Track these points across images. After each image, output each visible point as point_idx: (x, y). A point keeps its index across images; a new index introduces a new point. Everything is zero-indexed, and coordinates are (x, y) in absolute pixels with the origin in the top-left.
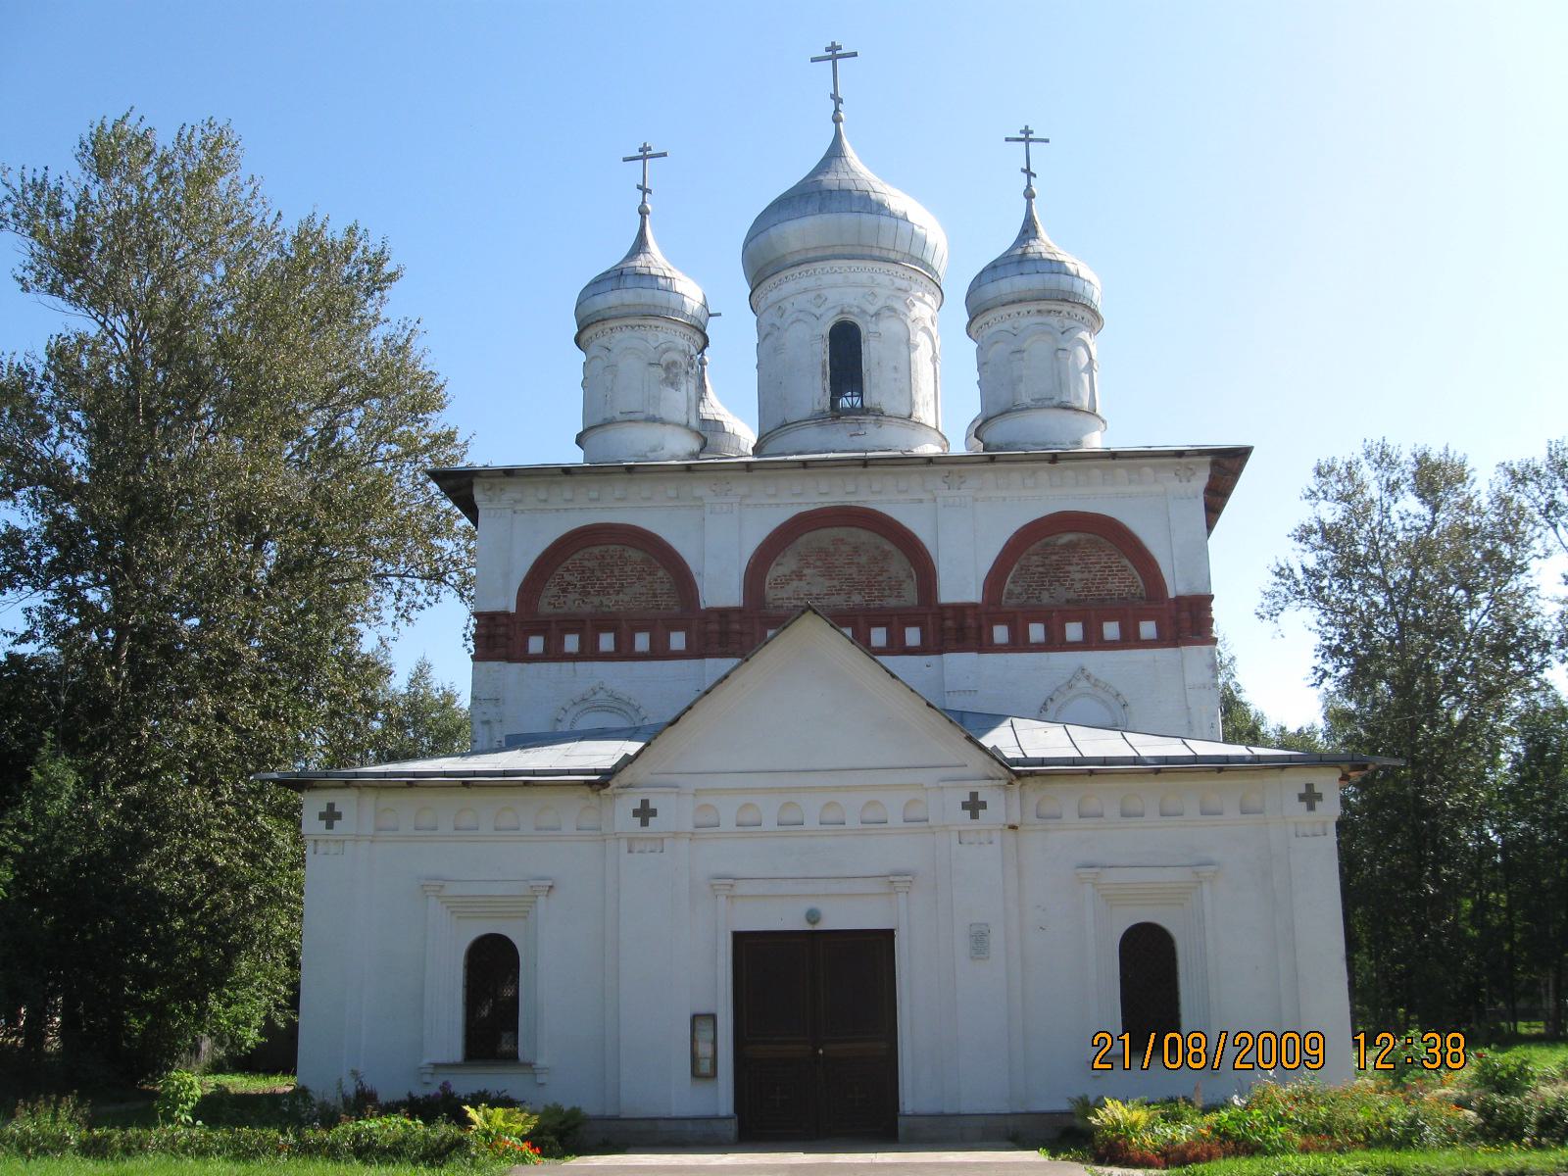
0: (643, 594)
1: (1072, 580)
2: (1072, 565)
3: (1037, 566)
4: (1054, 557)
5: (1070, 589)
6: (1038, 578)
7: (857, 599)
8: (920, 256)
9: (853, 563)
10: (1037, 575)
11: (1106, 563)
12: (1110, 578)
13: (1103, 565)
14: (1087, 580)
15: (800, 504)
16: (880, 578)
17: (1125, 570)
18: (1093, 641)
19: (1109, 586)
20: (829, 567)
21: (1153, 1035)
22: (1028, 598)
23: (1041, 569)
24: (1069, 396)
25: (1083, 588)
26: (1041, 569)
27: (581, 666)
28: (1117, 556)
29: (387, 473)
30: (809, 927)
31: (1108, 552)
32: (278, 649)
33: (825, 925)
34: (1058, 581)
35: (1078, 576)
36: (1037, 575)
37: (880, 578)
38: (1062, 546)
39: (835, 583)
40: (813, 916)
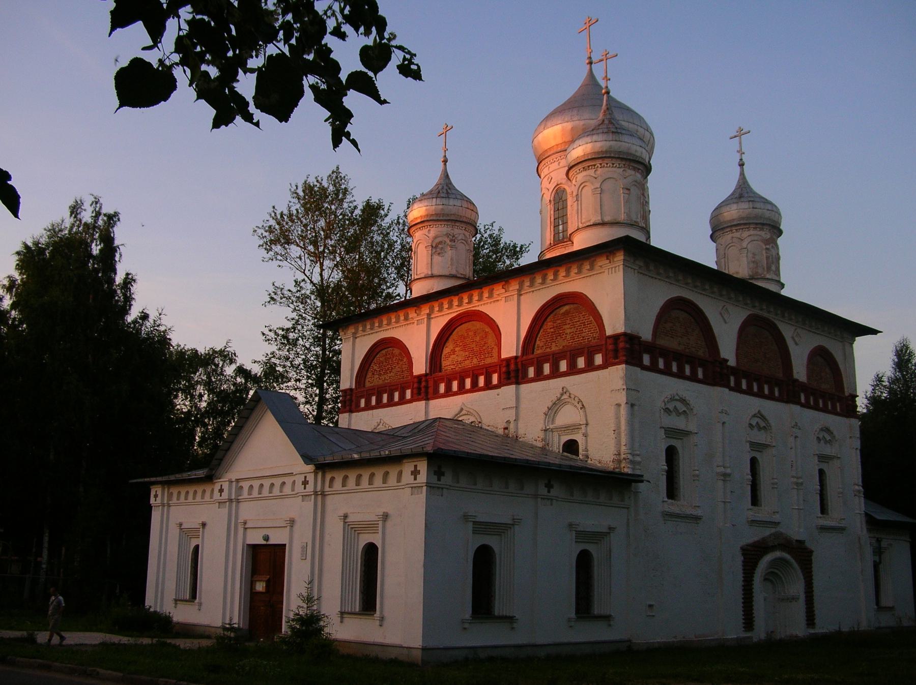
0: (398, 371)
1: (566, 334)
2: (566, 324)
3: (551, 328)
4: (559, 322)
5: (565, 339)
6: (551, 335)
7: (475, 361)
8: (470, 217)
9: (473, 341)
10: (550, 334)
11: (582, 320)
12: (584, 329)
13: (581, 322)
14: (573, 332)
15: (454, 312)
16: (484, 348)
17: (591, 323)
18: (573, 370)
19: (583, 335)
20: (465, 345)
21: (131, 481)
22: (546, 348)
23: (552, 330)
24: (624, 197)
25: (571, 338)
26: (552, 330)
27: (552, 381)
28: (587, 315)
29: (232, 383)
30: (264, 543)
31: (583, 314)
32: (403, 225)
33: (271, 542)
34: (560, 336)
35: (568, 331)
36: (550, 334)
37: (484, 348)
38: (562, 314)
39: (467, 353)
40: (266, 538)
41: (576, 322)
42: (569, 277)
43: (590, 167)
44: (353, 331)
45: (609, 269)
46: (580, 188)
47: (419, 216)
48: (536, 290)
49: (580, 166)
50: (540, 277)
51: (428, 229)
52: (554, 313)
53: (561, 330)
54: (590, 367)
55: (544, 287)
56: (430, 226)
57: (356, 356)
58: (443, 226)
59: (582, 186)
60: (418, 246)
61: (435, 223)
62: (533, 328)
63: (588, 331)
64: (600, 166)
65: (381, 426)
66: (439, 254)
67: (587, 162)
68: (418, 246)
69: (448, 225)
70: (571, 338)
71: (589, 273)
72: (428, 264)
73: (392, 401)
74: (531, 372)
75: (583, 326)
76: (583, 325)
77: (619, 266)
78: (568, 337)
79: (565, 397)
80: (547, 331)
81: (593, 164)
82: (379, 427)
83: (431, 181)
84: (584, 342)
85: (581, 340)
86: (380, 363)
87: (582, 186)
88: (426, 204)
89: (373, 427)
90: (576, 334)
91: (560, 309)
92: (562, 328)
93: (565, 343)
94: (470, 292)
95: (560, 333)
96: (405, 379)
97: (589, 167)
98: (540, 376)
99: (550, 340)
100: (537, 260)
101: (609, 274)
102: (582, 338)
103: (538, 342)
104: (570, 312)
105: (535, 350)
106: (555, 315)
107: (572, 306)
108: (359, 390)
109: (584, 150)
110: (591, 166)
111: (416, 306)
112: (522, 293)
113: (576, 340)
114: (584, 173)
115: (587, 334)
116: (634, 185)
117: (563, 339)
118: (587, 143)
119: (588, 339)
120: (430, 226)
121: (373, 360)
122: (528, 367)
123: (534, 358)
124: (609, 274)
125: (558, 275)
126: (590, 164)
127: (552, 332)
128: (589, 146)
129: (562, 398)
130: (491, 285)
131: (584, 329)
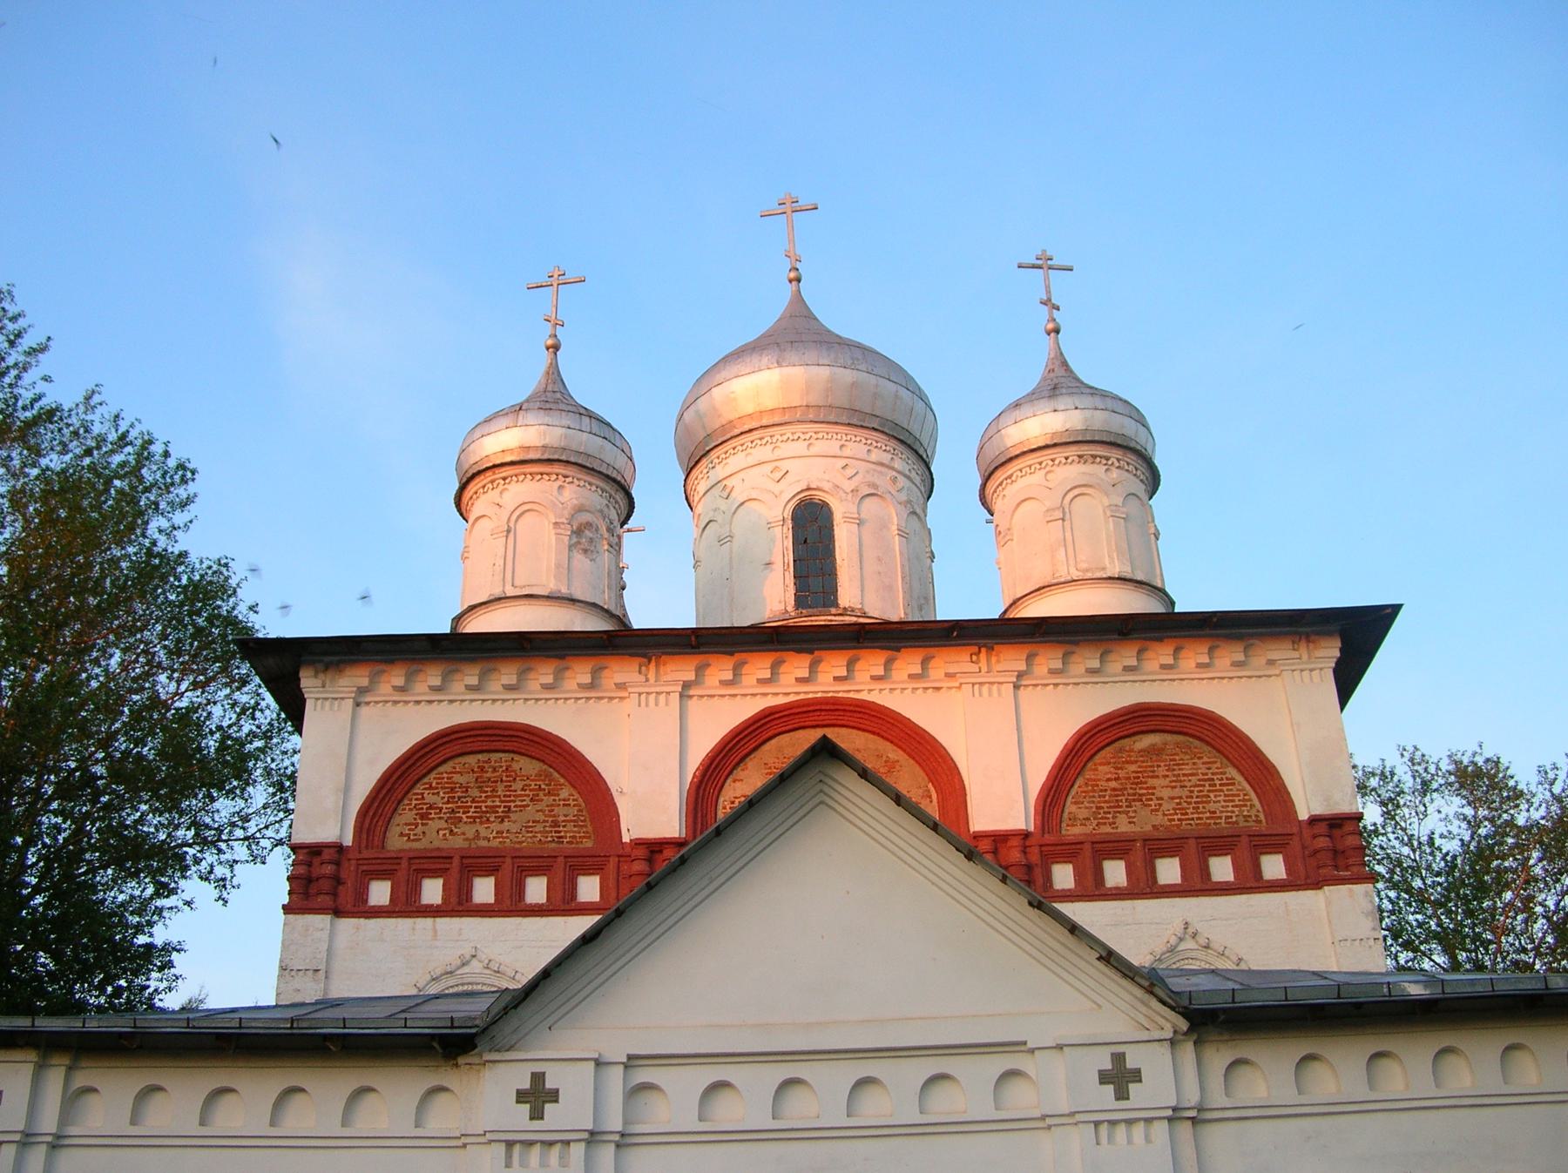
4: (1133, 768)
12: (1212, 795)
19: (1212, 806)
23: (1113, 784)
26: (1113, 784)
28: (1219, 765)
31: (1205, 759)
35: (1166, 793)
41: (1184, 775)
42: (1175, 671)
43: (1098, 459)
44: (365, 682)
45: (640, 694)
46: (517, 513)
47: (540, 445)
48: (1064, 684)
49: (1072, 451)
50: (367, 674)
51: (559, 483)
52: (1117, 745)
53: (1140, 788)
54: (1250, 882)
55: (1131, 678)
56: (566, 477)
57: (361, 755)
58: (594, 488)
59: (1076, 492)
60: (519, 517)
61: (580, 476)
62: (1066, 769)
63: (1225, 801)
64: (1117, 464)
65: (476, 966)
66: (585, 551)
67: (1092, 447)
68: (519, 517)
69: (603, 491)
70: (1174, 809)
71: (1050, 678)
72: (558, 566)
74: (380, 893)
75: (1207, 788)
76: (1207, 784)
77: (668, 693)
78: (1166, 806)
79: (1189, 944)
80: (1097, 785)
81: (1105, 454)
82: (466, 969)
83: (529, 380)
84: (1215, 824)
85: (1207, 818)
86: (452, 789)
87: (1076, 492)
88: (568, 423)
89: (1160, 948)
90: (1189, 803)
91: (1134, 738)
92: (1146, 783)
93: (1159, 819)
94: (855, 651)
95: (1140, 795)
96: (565, 845)
97: (1094, 457)
98: (406, 905)
99: (1110, 807)
100: (449, 631)
101: (639, 705)
102: (1208, 815)
103: (1070, 808)
104: (1163, 750)
105: (1064, 825)
106: (1121, 750)
107: (1168, 737)
108: (366, 854)
109: (1086, 420)
110: (1101, 457)
111: (644, 656)
112: (1024, 683)
113: (1191, 816)
114: (1082, 468)
115: (1223, 807)
117: (1152, 811)
118: (1096, 409)
119: (1227, 817)
120: (566, 477)
121: (424, 776)
122: (526, 876)
123: (1082, 843)
124: (639, 705)
125: (563, 679)
126: (1099, 453)
127: (1114, 789)
128: (559, 431)
129: (1180, 948)
130: (381, 662)
131: (1212, 795)
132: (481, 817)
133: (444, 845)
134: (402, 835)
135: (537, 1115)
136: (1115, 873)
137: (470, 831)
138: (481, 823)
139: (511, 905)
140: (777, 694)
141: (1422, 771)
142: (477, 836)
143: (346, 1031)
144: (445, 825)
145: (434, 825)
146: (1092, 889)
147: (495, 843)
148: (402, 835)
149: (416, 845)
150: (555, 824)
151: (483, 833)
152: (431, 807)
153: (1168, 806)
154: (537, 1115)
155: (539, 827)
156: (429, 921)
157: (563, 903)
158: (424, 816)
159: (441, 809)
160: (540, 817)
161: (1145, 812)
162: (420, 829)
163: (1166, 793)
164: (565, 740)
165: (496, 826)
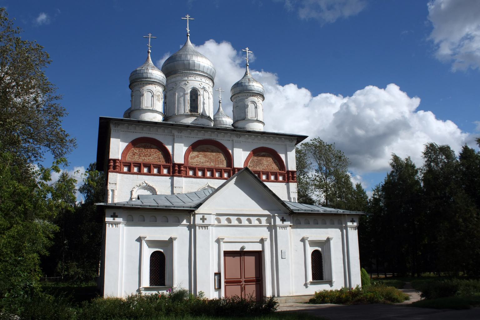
19: (272, 166)
23: (257, 161)
26: (257, 161)
73: (124, 165)
78: (265, 166)
96: (161, 163)
116: (251, 103)
127: (257, 162)
132: (145, 156)
133: (138, 160)
134: (130, 158)
135: (203, 222)
136: (208, 174)
137: (143, 158)
138: (145, 157)
139: (213, 177)
140: (199, 138)
141: (56, 149)
142: (144, 159)
143: (305, 212)
144: (138, 157)
145: (136, 156)
146: (268, 179)
147: (148, 161)
148: (130, 158)
149: (133, 160)
150: (159, 158)
151: (146, 159)
152: (135, 153)
153: (265, 166)
154: (203, 222)
155: (156, 159)
156: (136, 175)
157: (221, 177)
158: (134, 154)
159: (137, 153)
160: (156, 156)
161: (261, 166)
162: (133, 157)
163: (265, 163)
164: (262, 147)
165: (148, 158)
